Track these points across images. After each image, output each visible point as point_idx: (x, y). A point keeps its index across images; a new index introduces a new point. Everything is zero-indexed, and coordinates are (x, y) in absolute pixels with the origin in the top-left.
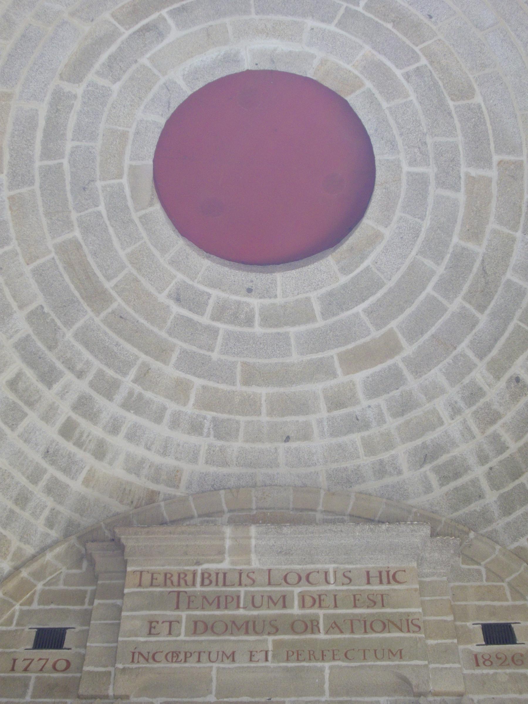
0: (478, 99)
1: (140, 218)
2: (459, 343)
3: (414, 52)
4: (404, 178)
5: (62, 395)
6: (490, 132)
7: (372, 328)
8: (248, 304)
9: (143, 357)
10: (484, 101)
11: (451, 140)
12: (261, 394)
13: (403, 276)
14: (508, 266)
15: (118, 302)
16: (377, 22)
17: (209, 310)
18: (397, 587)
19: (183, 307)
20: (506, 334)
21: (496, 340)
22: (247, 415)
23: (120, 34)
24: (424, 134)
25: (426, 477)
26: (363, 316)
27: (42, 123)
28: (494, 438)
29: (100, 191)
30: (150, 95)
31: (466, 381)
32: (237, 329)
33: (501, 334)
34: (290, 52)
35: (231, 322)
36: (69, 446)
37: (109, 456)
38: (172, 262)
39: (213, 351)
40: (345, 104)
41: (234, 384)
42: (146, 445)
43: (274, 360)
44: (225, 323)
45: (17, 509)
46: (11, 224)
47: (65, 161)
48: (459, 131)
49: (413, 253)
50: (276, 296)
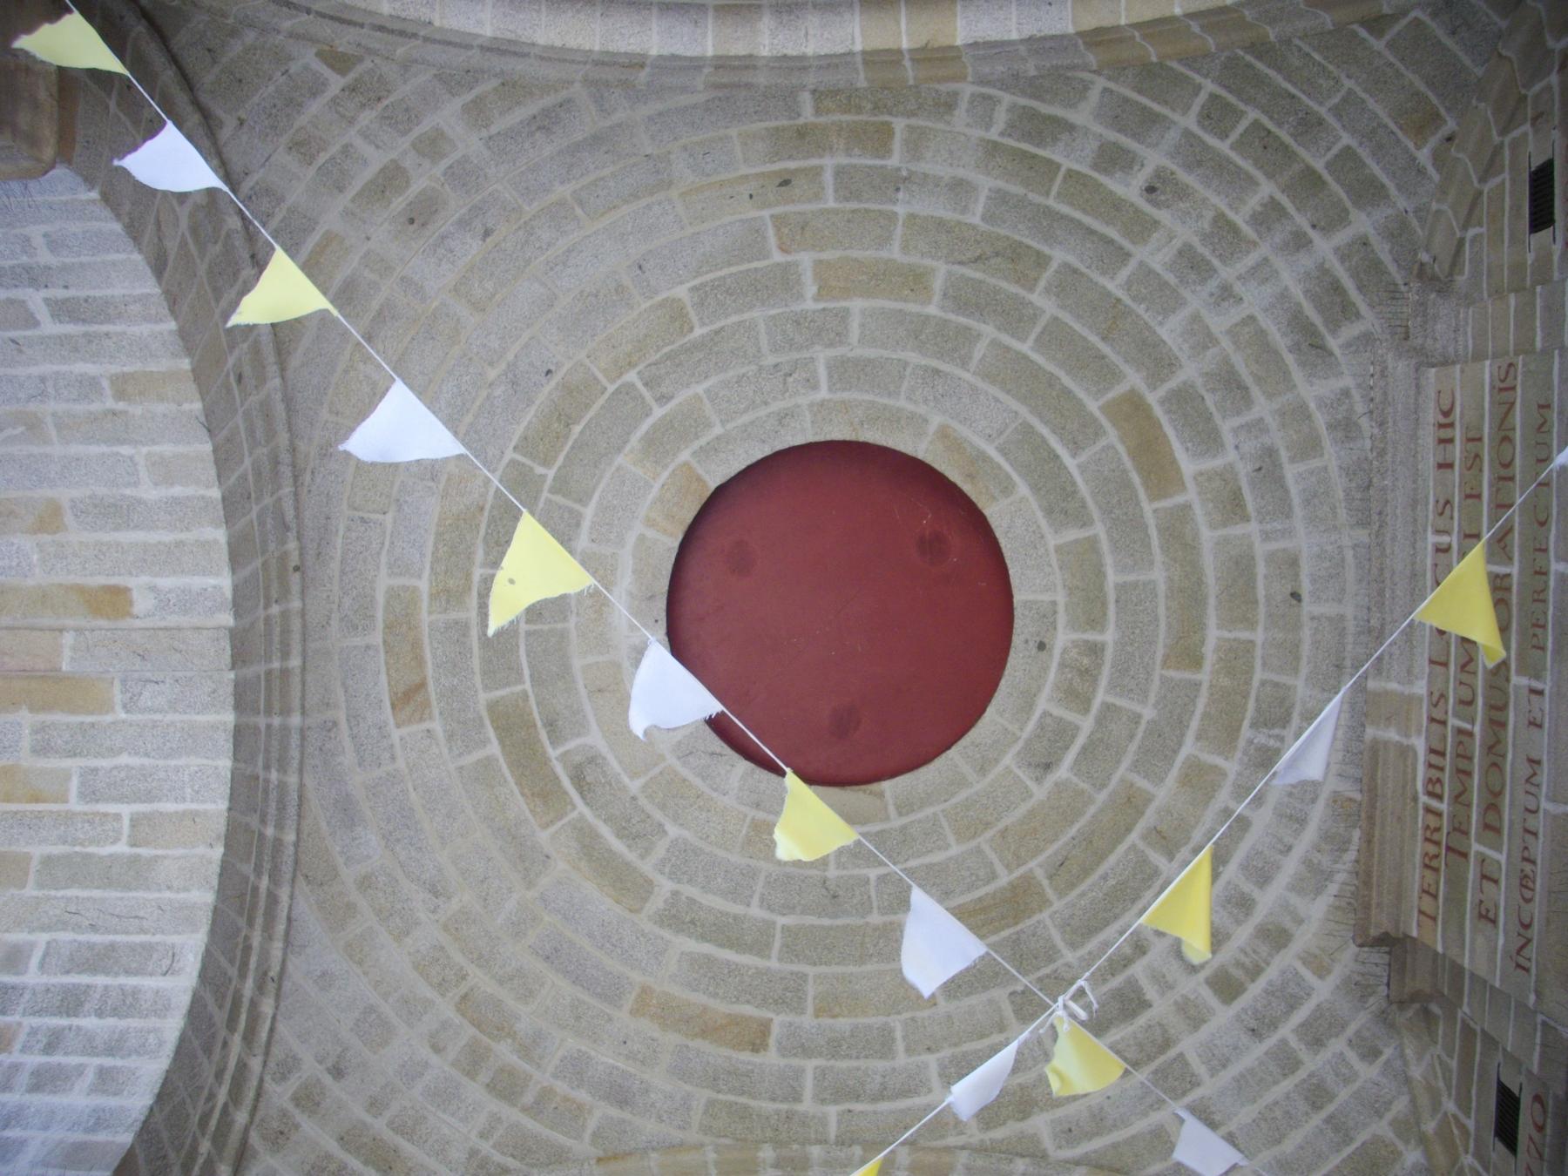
0: (682, 292)
1: (900, 814)
2: (1109, 294)
3: (617, 392)
4: (839, 396)
5: (1165, 986)
6: (733, 269)
7: (1103, 442)
8: (1065, 651)
9: (1134, 837)
10: (682, 283)
11: (762, 327)
12: (1218, 639)
13: (1008, 392)
14: (959, 223)
15: (1036, 866)
16: (573, 448)
17: (1070, 716)
18: (1458, 410)
19: (1059, 760)
20: (1078, 215)
21: (1092, 232)
22: (1253, 667)
23: (582, 818)
24: (761, 368)
25: (1348, 345)
26: (1084, 457)
27: (707, 948)
28: (1261, 224)
29: (845, 872)
30: (697, 782)
31: (1171, 279)
32: (1106, 671)
33: (1079, 224)
34: (634, 572)
35: (1095, 681)
36: (1255, 989)
37: (1287, 923)
38: (982, 770)
39: (1140, 716)
40: (721, 490)
41: (1197, 685)
42: (1281, 852)
43: (1162, 611)
44: (1094, 691)
45: (1330, 1108)
46: (862, 1020)
47: (781, 921)
48: (746, 316)
49: (967, 376)
50: (1054, 603)
